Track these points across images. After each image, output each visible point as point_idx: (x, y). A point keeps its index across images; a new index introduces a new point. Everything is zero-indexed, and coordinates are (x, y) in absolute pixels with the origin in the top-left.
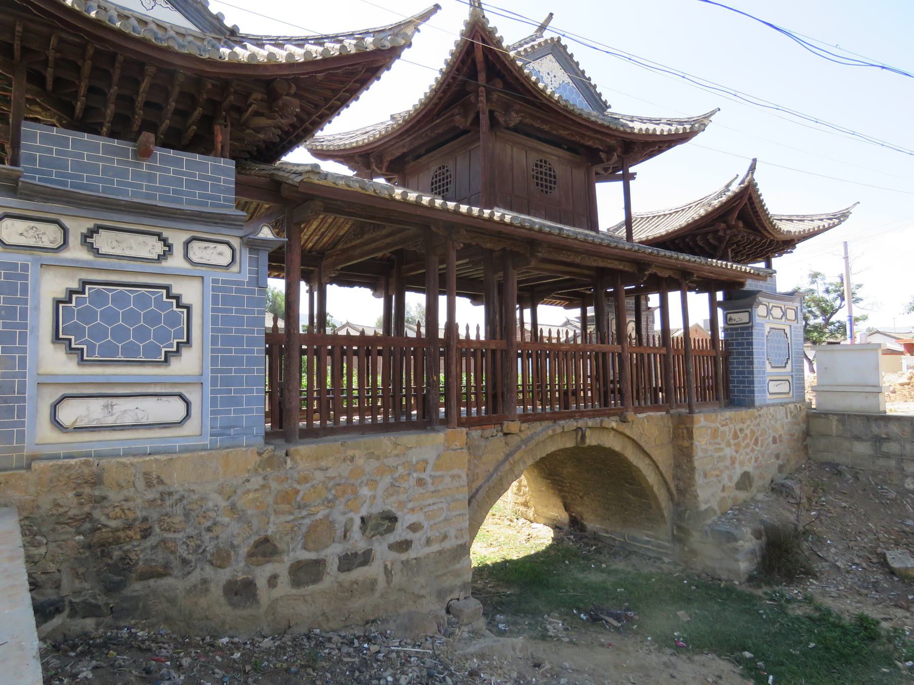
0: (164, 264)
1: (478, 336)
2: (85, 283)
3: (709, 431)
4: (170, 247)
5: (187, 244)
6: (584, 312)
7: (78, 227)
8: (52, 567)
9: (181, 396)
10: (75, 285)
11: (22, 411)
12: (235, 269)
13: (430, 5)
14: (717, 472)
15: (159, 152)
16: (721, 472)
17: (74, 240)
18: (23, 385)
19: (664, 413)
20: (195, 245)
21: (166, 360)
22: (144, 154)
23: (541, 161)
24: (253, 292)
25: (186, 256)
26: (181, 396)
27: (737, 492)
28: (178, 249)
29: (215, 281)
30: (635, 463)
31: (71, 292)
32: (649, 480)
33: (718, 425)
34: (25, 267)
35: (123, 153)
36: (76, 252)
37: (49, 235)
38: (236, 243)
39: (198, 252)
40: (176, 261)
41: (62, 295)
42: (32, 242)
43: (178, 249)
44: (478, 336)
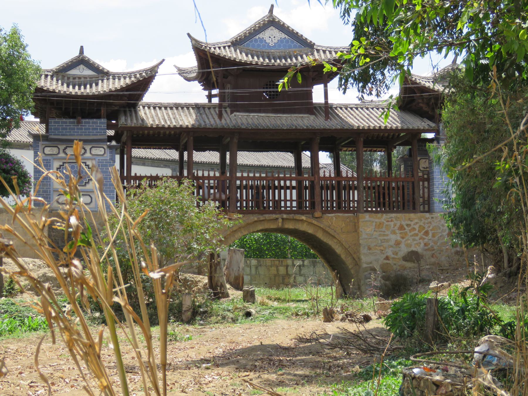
0: (84, 156)
1: (330, 175)
2: (64, 163)
3: (374, 224)
4: (86, 150)
5: (91, 149)
6: (298, 160)
7: (62, 147)
8: (57, 239)
9: (89, 195)
10: (61, 164)
11: (50, 197)
12: (105, 155)
13: (161, 60)
14: (382, 248)
15: (84, 121)
16: (385, 248)
17: (61, 151)
18: (50, 191)
19: (352, 215)
20: (93, 149)
21: (85, 185)
22: (79, 122)
23: (270, 82)
24: (110, 162)
25: (90, 153)
26: (89, 195)
27: (404, 262)
28: (88, 151)
29: (99, 160)
30: (325, 241)
31: (61, 166)
32: (337, 251)
33: (383, 220)
34: (50, 160)
35: (74, 123)
36: (62, 155)
37: (55, 150)
38: (105, 147)
39: (95, 151)
40: (88, 155)
41: (58, 167)
42: (51, 153)
43: (88, 151)
44: (330, 175)
